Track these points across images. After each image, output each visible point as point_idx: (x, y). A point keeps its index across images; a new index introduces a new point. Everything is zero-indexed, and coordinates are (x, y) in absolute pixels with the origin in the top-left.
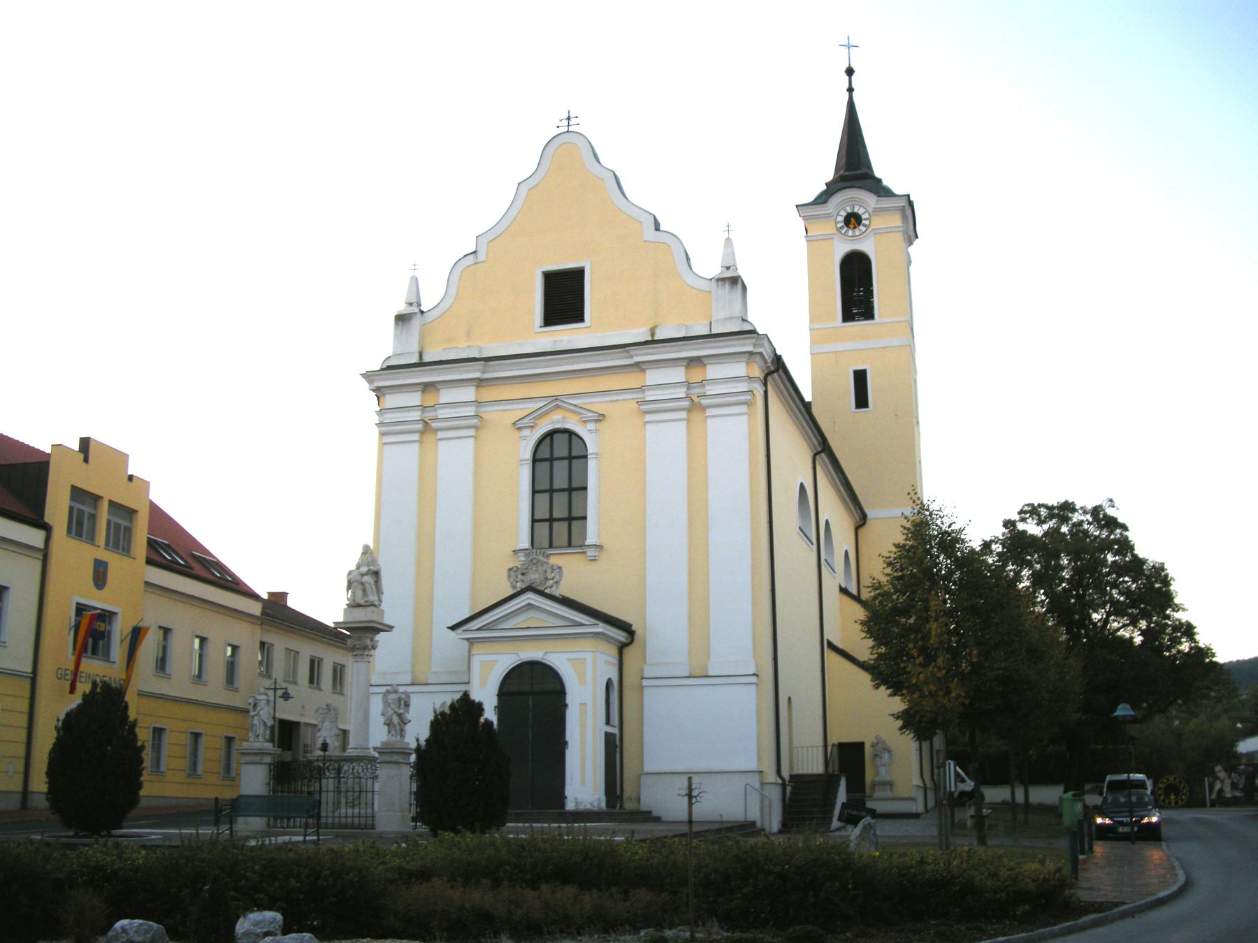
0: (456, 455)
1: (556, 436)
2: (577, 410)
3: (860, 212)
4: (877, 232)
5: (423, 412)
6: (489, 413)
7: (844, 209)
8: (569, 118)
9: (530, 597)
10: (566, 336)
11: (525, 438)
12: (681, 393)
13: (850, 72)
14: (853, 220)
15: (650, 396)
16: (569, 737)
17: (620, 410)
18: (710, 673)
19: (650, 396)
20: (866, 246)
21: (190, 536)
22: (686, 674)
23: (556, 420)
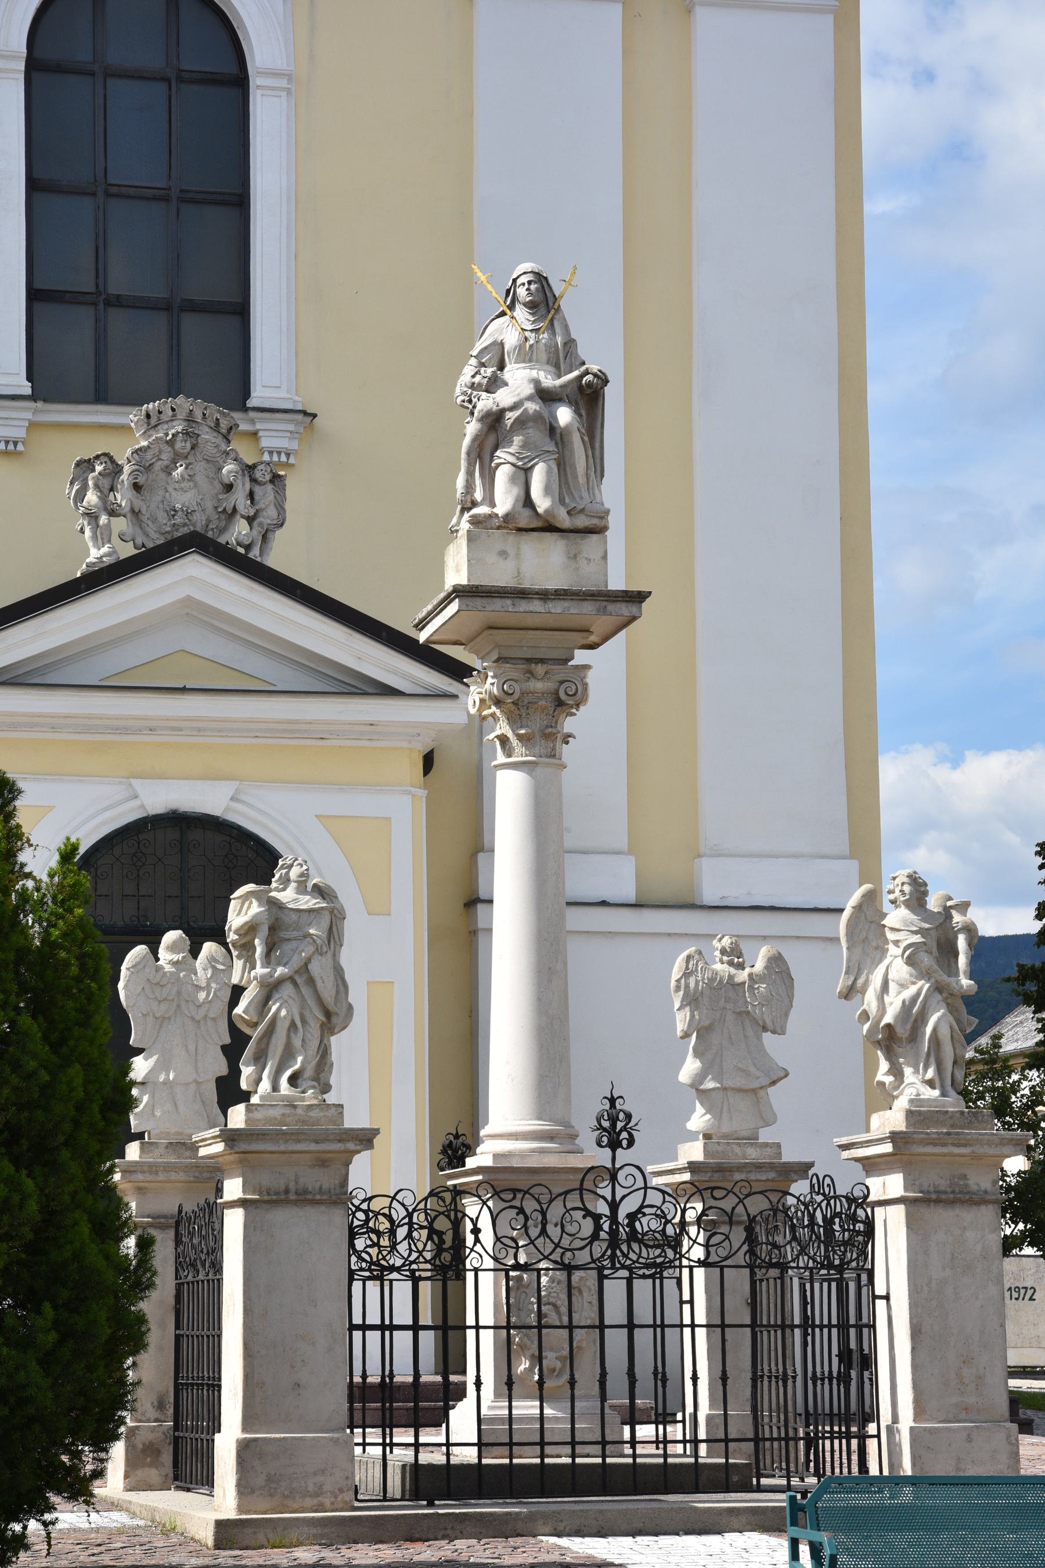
9: (194, 576)
18: (709, 896)
22: (629, 894)
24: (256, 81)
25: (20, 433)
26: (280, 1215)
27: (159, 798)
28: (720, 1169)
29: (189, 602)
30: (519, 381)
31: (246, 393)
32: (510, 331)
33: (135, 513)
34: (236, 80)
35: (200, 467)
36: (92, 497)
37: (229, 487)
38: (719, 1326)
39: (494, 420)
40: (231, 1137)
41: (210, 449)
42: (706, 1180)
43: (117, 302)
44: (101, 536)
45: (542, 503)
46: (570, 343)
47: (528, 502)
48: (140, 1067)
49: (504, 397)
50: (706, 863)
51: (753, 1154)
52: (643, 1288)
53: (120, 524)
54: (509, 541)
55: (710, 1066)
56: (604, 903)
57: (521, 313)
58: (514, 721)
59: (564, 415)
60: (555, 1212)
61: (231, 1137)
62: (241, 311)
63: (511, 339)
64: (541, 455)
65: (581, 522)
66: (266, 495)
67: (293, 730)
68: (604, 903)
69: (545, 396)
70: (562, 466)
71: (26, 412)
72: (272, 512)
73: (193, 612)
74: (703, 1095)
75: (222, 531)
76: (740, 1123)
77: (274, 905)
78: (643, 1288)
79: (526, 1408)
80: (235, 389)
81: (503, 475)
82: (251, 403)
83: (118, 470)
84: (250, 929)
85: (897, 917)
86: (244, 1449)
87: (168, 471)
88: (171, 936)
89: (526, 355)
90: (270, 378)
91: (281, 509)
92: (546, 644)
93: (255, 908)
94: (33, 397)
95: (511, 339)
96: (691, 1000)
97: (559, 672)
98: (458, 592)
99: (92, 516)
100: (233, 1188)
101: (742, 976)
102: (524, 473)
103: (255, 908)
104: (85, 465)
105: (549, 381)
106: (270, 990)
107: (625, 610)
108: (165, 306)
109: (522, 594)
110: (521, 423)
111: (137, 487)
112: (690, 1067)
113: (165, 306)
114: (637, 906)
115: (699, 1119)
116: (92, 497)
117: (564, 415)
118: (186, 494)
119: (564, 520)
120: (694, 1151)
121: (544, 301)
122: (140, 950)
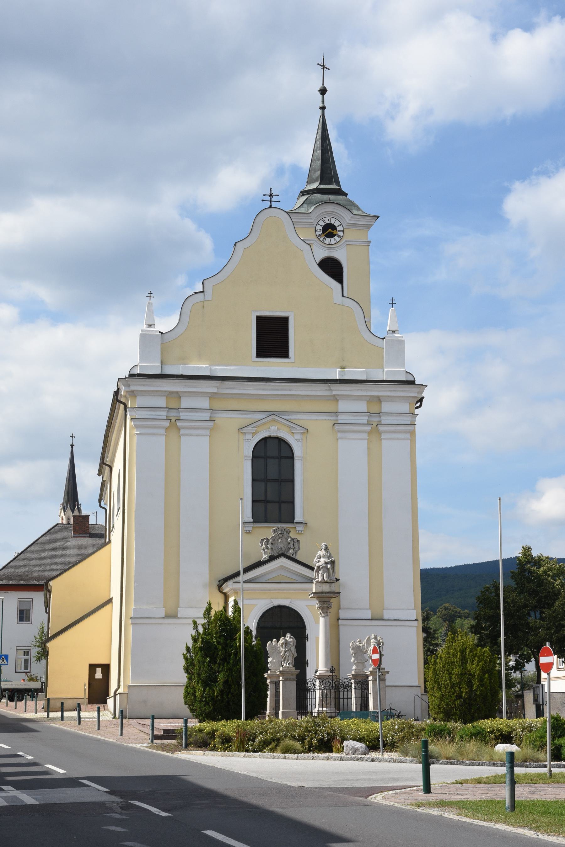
0: (195, 448)
1: (268, 440)
2: (292, 425)
3: (336, 224)
4: (349, 244)
5: (168, 412)
6: (220, 417)
7: (323, 219)
8: (271, 195)
9: (282, 561)
10: (272, 367)
11: (249, 440)
12: (364, 419)
13: (323, 91)
14: (329, 231)
15: (342, 419)
16: (308, 657)
17: (319, 426)
18: (386, 618)
19: (342, 419)
20: (340, 254)
21: (475, 565)
22: (369, 617)
23: (274, 431)
24: (295, 458)
25: (251, 529)
26: (287, 682)
27: (276, 603)
28: (356, 675)
29: (281, 566)
30: (322, 560)
31: (294, 519)
32: (321, 553)
33: (272, 549)
34: (292, 457)
35: (284, 540)
36: (264, 546)
37: (289, 543)
38: (356, 697)
39: (319, 567)
40: (280, 672)
41: (286, 536)
42: (355, 677)
43: (269, 502)
44: (265, 553)
45: (325, 579)
46: (330, 554)
47: (323, 579)
48: (270, 660)
49: (320, 564)
50: (385, 611)
51: (362, 673)
52: (345, 693)
53: (269, 551)
54: (321, 585)
55: (356, 658)
56: (364, 619)
57: (323, 550)
58: (322, 611)
59: (329, 566)
60: (324, 682)
61: (280, 672)
62: (293, 502)
63: (322, 554)
64: (325, 572)
65: (331, 581)
66: (296, 544)
67: (301, 589)
68: (364, 619)
69: (326, 563)
70: (329, 573)
71: (252, 525)
72: (297, 548)
73: (282, 567)
74: (355, 663)
75: (288, 551)
76: (361, 668)
77: (286, 640)
78: (345, 693)
79: (325, 709)
80: (291, 519)
81: (320, 575)
82: (295, 521)
83: (268, 541)
84: (283, 644)
85: (373, 641)
86: (282, 712)
87: (278, 540)
88: (274, 640)
89: (324, 557)
90: (298, 517)
91: (299, 547)
92: (326, 599)
93: (283, 641)
94: (253, 522)
95: (322, 554)
96: (353, 649)
97: (328, 603)
98: (313, 593)
99: (264, 550)
100: (281, 678)
101: (361, 645)
102: (323, 575)
103: (283, 641)
104: (263, 540)
105: (327, 561)
106: (285, 652)
107: (337, 595)
108: (278, 502)
109: (322, 593)
110: (322, 568)
111: (272, 544)
112: (353, 659)
113: (278, 502)
114: (371, 620)
115: (354, 667)
116: (264, 546)
117: (329, 566)
118: (281, 545)
119: (329, 581)
120: (353, 672)
121: (326, 549)
122: (270, 642)
